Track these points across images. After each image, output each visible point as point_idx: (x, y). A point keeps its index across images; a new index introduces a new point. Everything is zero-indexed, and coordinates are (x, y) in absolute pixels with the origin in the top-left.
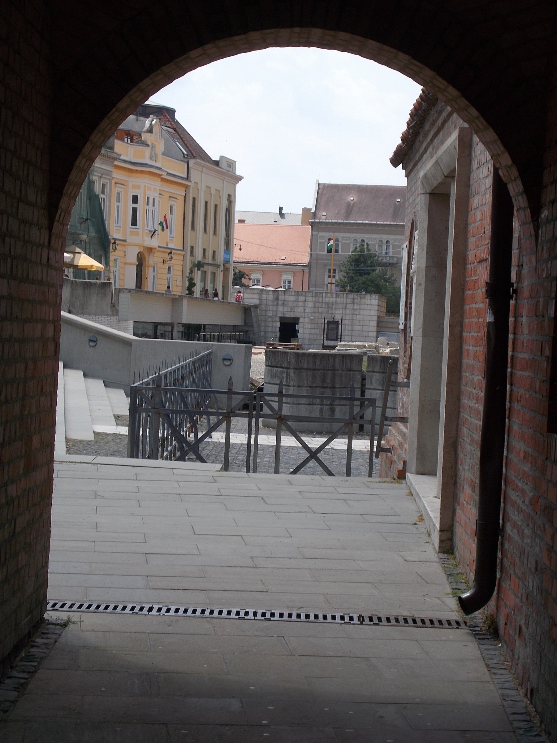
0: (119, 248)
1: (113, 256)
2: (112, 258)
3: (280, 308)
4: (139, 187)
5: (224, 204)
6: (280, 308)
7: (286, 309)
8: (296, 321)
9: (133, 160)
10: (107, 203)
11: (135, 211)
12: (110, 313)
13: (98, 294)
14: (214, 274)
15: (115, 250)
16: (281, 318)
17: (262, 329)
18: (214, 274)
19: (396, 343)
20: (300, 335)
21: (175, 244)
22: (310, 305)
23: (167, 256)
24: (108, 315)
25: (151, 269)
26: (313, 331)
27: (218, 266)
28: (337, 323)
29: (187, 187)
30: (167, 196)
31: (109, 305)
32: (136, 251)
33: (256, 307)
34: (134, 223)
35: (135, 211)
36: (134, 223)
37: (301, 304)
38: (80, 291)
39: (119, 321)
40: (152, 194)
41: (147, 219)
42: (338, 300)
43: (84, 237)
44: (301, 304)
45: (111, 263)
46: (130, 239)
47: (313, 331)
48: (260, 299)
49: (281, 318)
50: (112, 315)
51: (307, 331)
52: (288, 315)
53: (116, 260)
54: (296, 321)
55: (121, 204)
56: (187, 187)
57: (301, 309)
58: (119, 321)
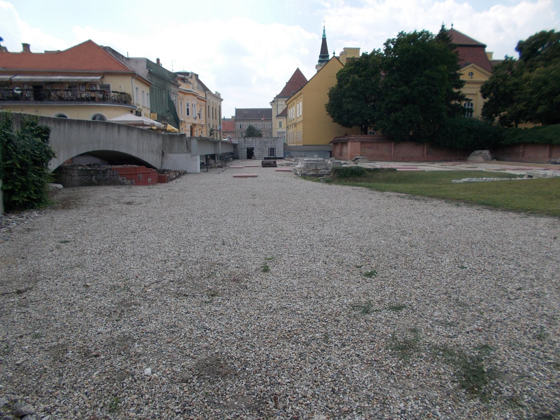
0: (183, 124)
1: (181, 127)
2: (180, 128)
3: (247, 144)
4: (189, 100)
5: (218, 109)
6: (247, 144)
7: (249, 144)
8: (253, 149)
9: (186, 89)
10: (177, 105)
11: (188, 109)
12: (186, 152)
13: (178, 142)
14: (216, 133)
15: (181, 125)
16: (247, 148)
17: (240, 152)
18: (216, 133)
19: (320, 159)
20: (255, 154)
21: (203, 123)
22: (258, 142)
23: (201, 127)
24: (185, 153)
25: (195, 132)
26: (260, 152)
27: (218, 131)
28: (274, 149)
29: (206, 101)
30: (199, 104)
31: (185, 147)
32: (190, 125)
33: (238, 144)
34: (188, 114)
35: (188, 109)
36: (188, 114)
37: (254, 142)
38: (168, 140)
39: (192, 156)
40: (195, 103)
41: (193, 112)
42: (269, 140)
43: (168, 118)
44: (254, 142)
45: (181, 130)
46: (187, 121)
47: (260, 152)
48: (239, 141)
49: (247, 148)
50: (188, 153)
51: (257, 152)
52: (250, 147)
53: (182, 129)
54: (253, 149)
55: (183, 106)
56: (206, 101)
57: (254, 144)
58: (192, 156)
